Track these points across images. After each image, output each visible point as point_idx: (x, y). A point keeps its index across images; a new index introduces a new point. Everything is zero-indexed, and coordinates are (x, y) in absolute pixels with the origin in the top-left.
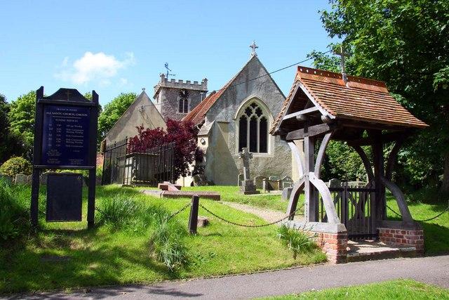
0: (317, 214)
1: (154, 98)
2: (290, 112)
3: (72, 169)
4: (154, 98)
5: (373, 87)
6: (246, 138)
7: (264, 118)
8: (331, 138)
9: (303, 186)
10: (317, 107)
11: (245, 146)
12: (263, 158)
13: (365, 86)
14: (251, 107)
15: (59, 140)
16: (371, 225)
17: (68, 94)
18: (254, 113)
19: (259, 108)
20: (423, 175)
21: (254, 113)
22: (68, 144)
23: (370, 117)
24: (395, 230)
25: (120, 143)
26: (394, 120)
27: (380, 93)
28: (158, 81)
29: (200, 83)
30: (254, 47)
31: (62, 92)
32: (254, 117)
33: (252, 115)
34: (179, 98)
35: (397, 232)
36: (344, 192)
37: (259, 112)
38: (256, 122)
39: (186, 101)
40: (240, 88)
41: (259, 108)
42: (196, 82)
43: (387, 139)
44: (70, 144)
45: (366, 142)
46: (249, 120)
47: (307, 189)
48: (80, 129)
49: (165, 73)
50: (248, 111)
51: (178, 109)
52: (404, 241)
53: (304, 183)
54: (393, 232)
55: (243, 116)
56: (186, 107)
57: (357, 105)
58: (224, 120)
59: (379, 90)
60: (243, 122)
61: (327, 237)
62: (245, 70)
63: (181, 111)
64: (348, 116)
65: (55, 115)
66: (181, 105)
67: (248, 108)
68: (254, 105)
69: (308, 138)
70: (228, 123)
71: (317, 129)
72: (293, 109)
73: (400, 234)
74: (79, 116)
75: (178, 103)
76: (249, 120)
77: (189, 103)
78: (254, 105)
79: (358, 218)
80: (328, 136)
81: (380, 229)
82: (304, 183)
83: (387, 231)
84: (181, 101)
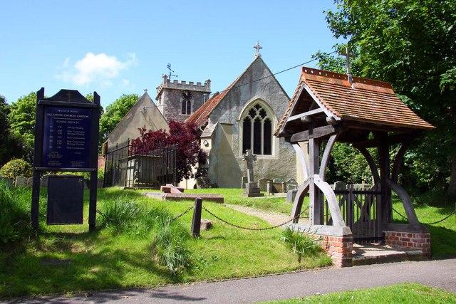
0: (322, 217)
1: (157, 99)
2: (294, 113)
3: (73, 171)
4: (157, 99)
5: (379, 89)
6: (250, 140)
7: (268, 119)
8: (336, 140)
9: (308, 188)
10: (322, 109)
11: (249, 148)
12: (267, 161)
13: (371, 87)
14: (255, 109)
15: (60, 142)
16: (377, 228)
17: (69, 95)
18: (258, 115)
19: (263, 110)
20: (430, 178)
21: (258, 115)
22: (69, 146)
23: (376, 118)
24: (401, 233)
25: (122, 144)
26: (401, 122)
27: (386, 94)
28: (160, 82)
29: (203, 85)
30: (258, 48)
31: (63, 93)
32: (258, 118)
33: (256, 116)
34: (181, 100)
35: (403, 235)
36: (349, 195)
37: (263, 113)
38: (260, 124)
39: (189, 102)
40: (244, 89)
41: (263, 110)
42: (199, 83)
43: (393, 141)
44: (71, 146)
45: (371, 144)
46: (253, 121)
47: (312, 192)
48: (81, 130)
49: (168, 74)
50: (252, 113)
51: (180, 110)
52: (410, 244)
53: (309, 186)
54: (399, 235)
55: (247, 118)
56: (189, 109)
57: (363, 107)
58: (227, 122)
59: (385, 91)
60: (246, 123)
61: (332, 240)
62: (249, 71)
63: (184, 113)
64: (353, 118)
65: (56, 117)
66: (184, 106)
67: (252, 109)
68: (258, 106)
69: (313, 139)
70: (232, 125)
71: (322, 131)
72: (297, 110)
73: (406, 237)
74: (80, 118)
75: (181, 104)
76: (253, 121)
77: (192, 105)
78: (258, 106)
79: (364, 221)
80: (333, 137)
81: (385, 232)
82: (309, 186)
83: (393, 234)
84: (184, 102)
